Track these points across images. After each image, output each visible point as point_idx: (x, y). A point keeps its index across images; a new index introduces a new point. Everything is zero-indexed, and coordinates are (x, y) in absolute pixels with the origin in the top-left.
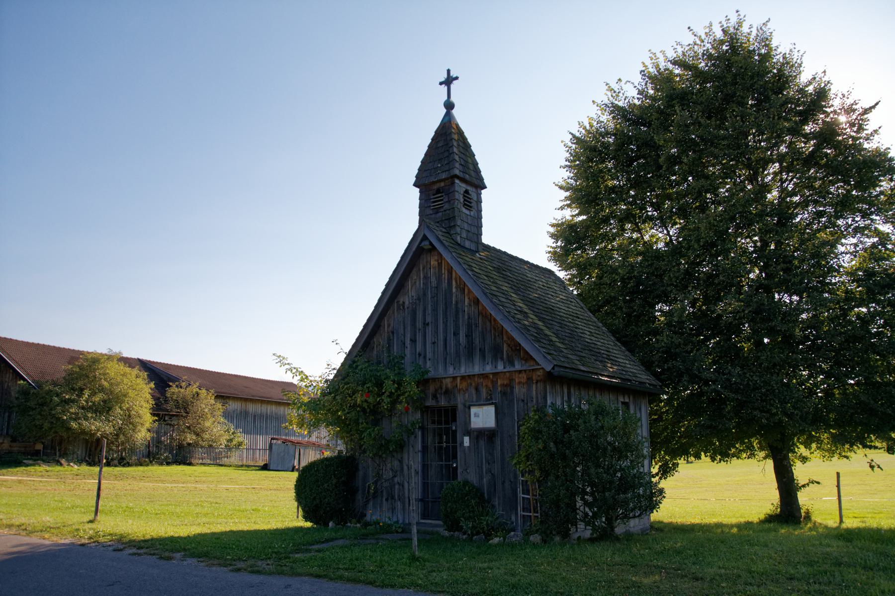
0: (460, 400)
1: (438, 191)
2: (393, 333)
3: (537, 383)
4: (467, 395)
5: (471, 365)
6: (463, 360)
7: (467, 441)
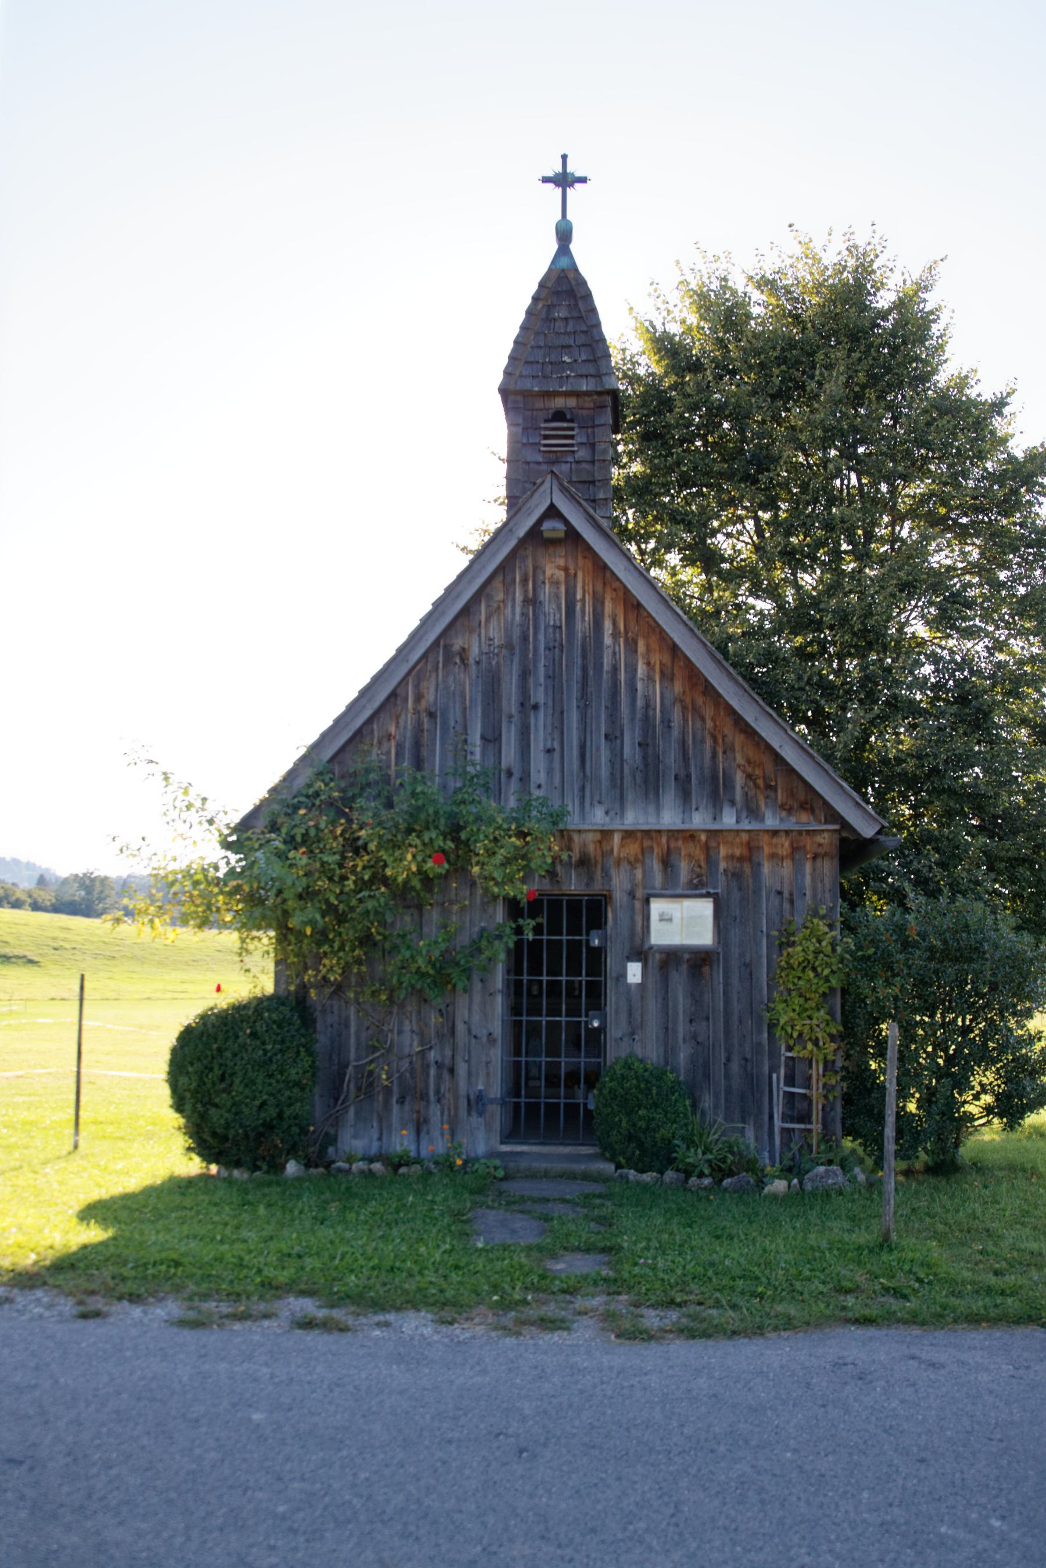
0: (619, 883)
1: (559, 415)
2: (432, 715)
3: (814, 858)
4: (639, 873)
5: (651, 809)
6: (630, 796)
7: (634, 972)
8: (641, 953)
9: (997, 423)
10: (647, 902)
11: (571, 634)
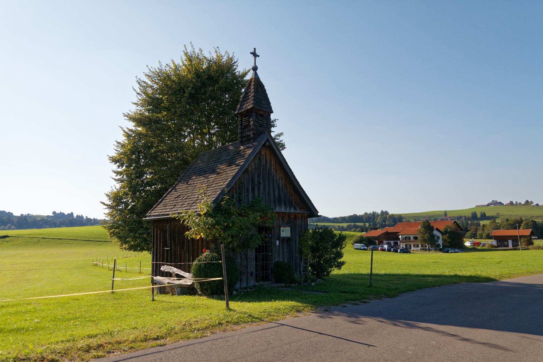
6: (277, 205)
8: (279, 238)
9: (467, 217)
10: (280, 228)
11: (266, 168)
